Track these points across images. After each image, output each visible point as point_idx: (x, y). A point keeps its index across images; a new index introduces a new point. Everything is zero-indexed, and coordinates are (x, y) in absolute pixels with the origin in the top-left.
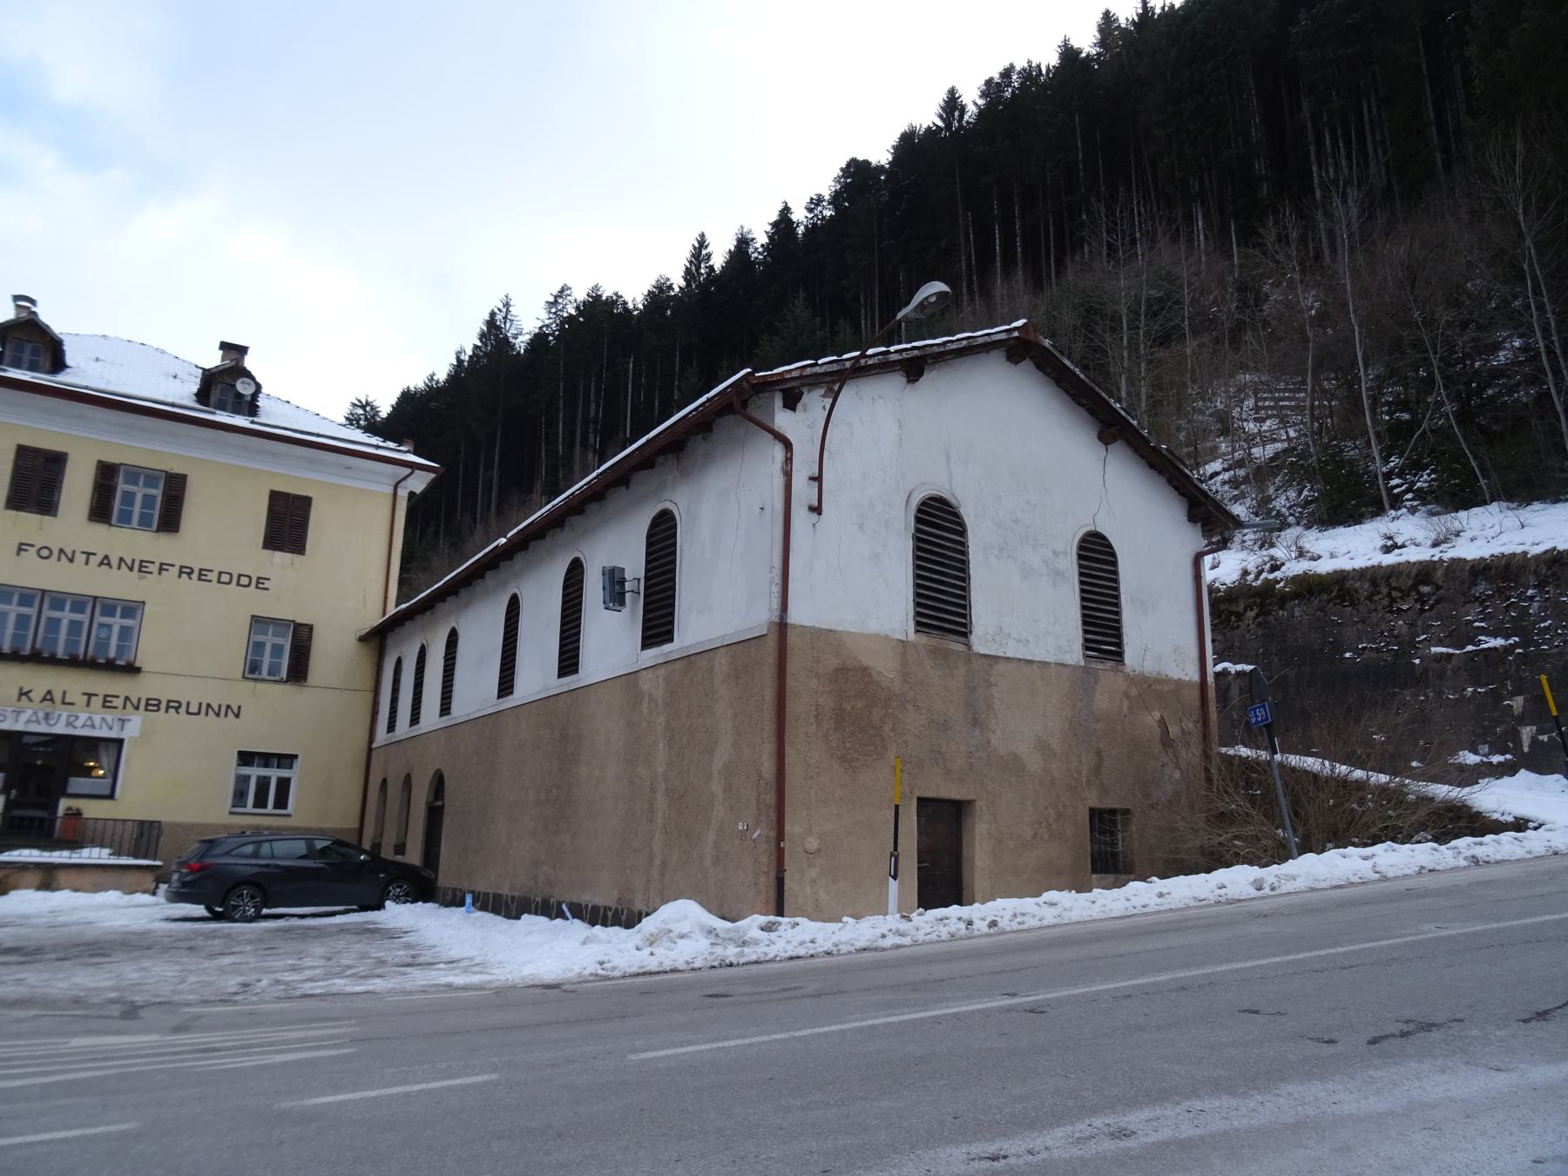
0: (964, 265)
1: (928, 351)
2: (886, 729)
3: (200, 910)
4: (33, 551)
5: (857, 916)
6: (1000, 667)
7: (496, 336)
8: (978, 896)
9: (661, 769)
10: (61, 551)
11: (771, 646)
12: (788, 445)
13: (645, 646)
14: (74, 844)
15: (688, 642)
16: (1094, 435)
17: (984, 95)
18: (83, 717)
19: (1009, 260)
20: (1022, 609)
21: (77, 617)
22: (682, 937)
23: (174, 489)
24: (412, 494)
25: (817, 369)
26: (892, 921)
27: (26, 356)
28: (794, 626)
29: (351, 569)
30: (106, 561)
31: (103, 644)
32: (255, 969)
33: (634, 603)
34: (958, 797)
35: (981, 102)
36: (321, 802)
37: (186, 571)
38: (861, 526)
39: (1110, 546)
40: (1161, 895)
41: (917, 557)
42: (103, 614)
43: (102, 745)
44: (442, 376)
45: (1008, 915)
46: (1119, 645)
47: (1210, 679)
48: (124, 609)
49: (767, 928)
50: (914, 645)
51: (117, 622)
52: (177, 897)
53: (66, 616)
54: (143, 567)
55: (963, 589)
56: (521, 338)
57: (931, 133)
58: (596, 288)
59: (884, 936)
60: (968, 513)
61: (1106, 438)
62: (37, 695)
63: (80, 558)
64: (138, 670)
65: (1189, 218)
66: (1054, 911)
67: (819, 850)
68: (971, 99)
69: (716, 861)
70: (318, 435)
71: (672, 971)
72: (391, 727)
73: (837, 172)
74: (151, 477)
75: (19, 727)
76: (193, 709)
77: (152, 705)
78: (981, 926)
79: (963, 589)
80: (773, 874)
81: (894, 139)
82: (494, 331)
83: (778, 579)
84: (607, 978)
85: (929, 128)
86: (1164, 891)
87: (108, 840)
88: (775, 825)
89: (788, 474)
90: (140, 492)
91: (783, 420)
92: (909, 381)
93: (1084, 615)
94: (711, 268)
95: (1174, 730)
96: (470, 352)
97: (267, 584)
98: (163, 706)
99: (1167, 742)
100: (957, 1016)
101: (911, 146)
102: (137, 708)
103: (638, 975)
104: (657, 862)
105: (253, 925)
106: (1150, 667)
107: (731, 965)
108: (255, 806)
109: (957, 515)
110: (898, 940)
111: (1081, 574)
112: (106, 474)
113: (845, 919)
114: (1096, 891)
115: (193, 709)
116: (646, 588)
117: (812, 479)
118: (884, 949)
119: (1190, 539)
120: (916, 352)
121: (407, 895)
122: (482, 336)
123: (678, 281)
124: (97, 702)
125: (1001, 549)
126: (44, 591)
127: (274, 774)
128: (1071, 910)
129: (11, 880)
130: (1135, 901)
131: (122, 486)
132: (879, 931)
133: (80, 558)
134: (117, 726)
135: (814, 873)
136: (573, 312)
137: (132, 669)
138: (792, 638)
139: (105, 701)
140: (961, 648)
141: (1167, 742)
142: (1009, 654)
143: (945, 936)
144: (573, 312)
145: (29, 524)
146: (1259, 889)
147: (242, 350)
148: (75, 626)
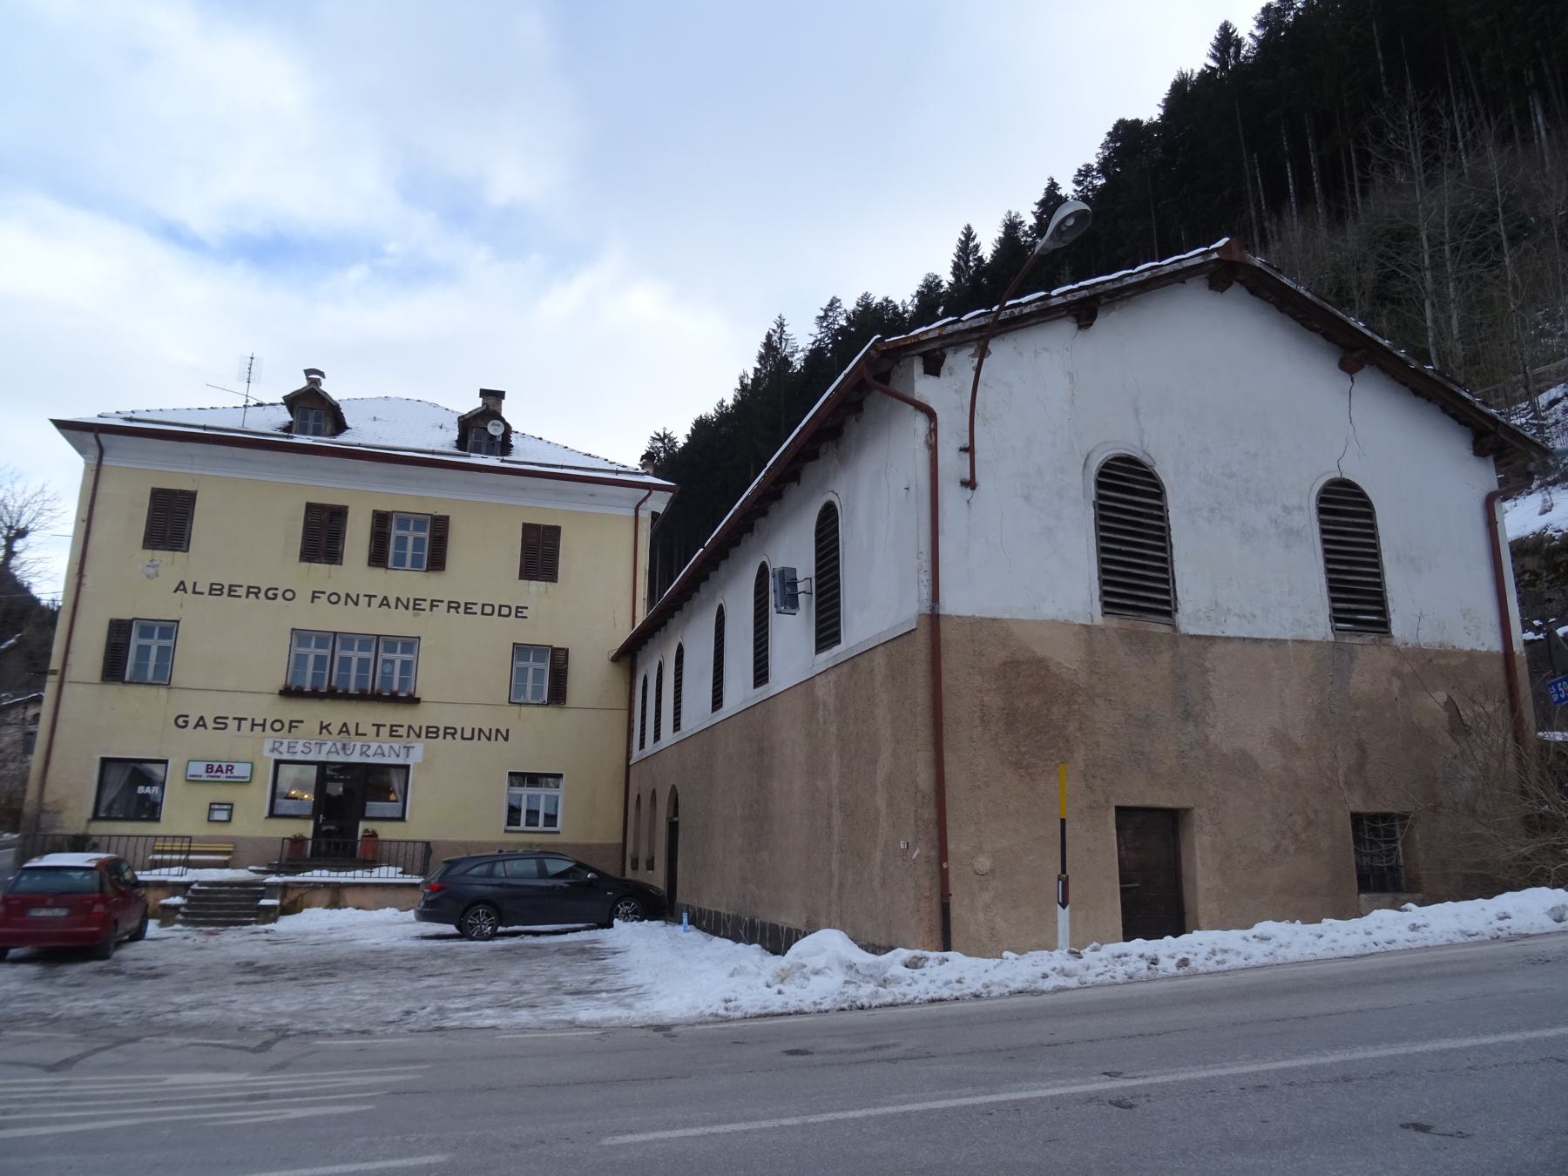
0: (1253, 214)
1: (1100, 289)
2: (1071, 728)
3: (451, 929)
5: (1020, 951)
6: (1217, 649)
7: (774, 357)
8: (1202, 922)
9: (835, 783)
10: (348, 595)
11: (922, 639)
12: (931, 415)
13: (819, 650)
14: (370, 864)
15: (852, 644)
16: (1335, 364)
17: (1261, 24)
18: (374, 746)
19: (1305, 196)
20: (1246, 578)
21: (365, 655)
22: (817, 973)
23: (439, 528)
24: (654, 515)
25: (959, 326)
26: (1060, 958)
27: (311, 423)
28: (949, 617)
29: (601, 591)
30: (385, 602)
31: (387, 678)
32: (408, 996)
33: (809, 604)
34: (1169, 805)
35: (1258, 33)
36: (585, 819)
37: (453, 606)
38: (1027, 498)
39: (1363, 494)
40: (1414, 928)
41: (1100, 528)
42: (343, 648)
43: (393, 771)
44: (729, 402)
45: (1206, 949)
46: (1383, 612)
47: (1518, 648)
48: (404, 644)
49: (913, 964)
50: (1103, 630)
51: (398, 657)
52: (424, 916)
53: (355, 655)
54: (416, 605)
55: (1164, 560)
56: (797, 356)
57: (1206, 76)
58: (866, 296)
59: (1045, 976)
60: (1166, 472)
61: (1349, 366)
62: (335, 729)
64: (418, 701)
65: (1525, 116)
66: (1266, 947)
67: (992, 871)
68: (1247, 29)
69: (883, 885)
70: (562, 467)
71: (797, 1013)
72: (642, 746)
73: (1103, 138)
74: (419, 521)
76: (468, 734)
77: (432, 732)
78: (1168, 966)
79: (1164, 560)
80: (936, 899)
81: (1163, 90)
82: (772, 351)
83: (927, 566)
84: (727, 1020)
85: (1203, 73)
86: (1419, 922)
87: (401, 860)
88: (936, 843)
89: (933, 448)
90: (411, 535)
91: (925, 388)
92: (1080, 327)
93: (1330, 580)
94: (980, 259)
95: (1467, 714)
96: (751, 376)
98: (441, 733)
99: (1458, 726)
100: (1017, 1106)
101: (1183, 95)
102: (419, 736)
103: (760, 1016)
104: (836, 884)
105: (490, 943)
106: (1428, 637)
107: (862, 1008)
108: (528, 824)
109: (1151, 475)
110: (1061, 981)
111: (1323, 531)
112: (381, 521)
113: (1005, 954)
114: (1326, 921)
115: (468, 734)
116: (818, 587)
117: (963, 450)
118: (1043, 992)
119: (1484, 477)
120: (1084, 293)
121: (635, 912)
122: (761, 358)
123: (947, 278)
124: (385, 731)
125: (1213, 510)
126: (335, 634)
128: (1288, 945)
129: (306, 898)
130: (1380, 936)
131: (395, 532)
132: (1040, 970)
133: (363, 601)
134: (403, 752)
135: (987, 897)
136: (844, 323)
137: (413, 700)
138: (947, 631)
140: (1164, 629)
141: (1458, 726)
142: (1229, 633)
143: (1120, 978)
144: (844, 323)
145: (320, 573)
146: (1559, 920)
147: (499, 395)
148: (363, 663)
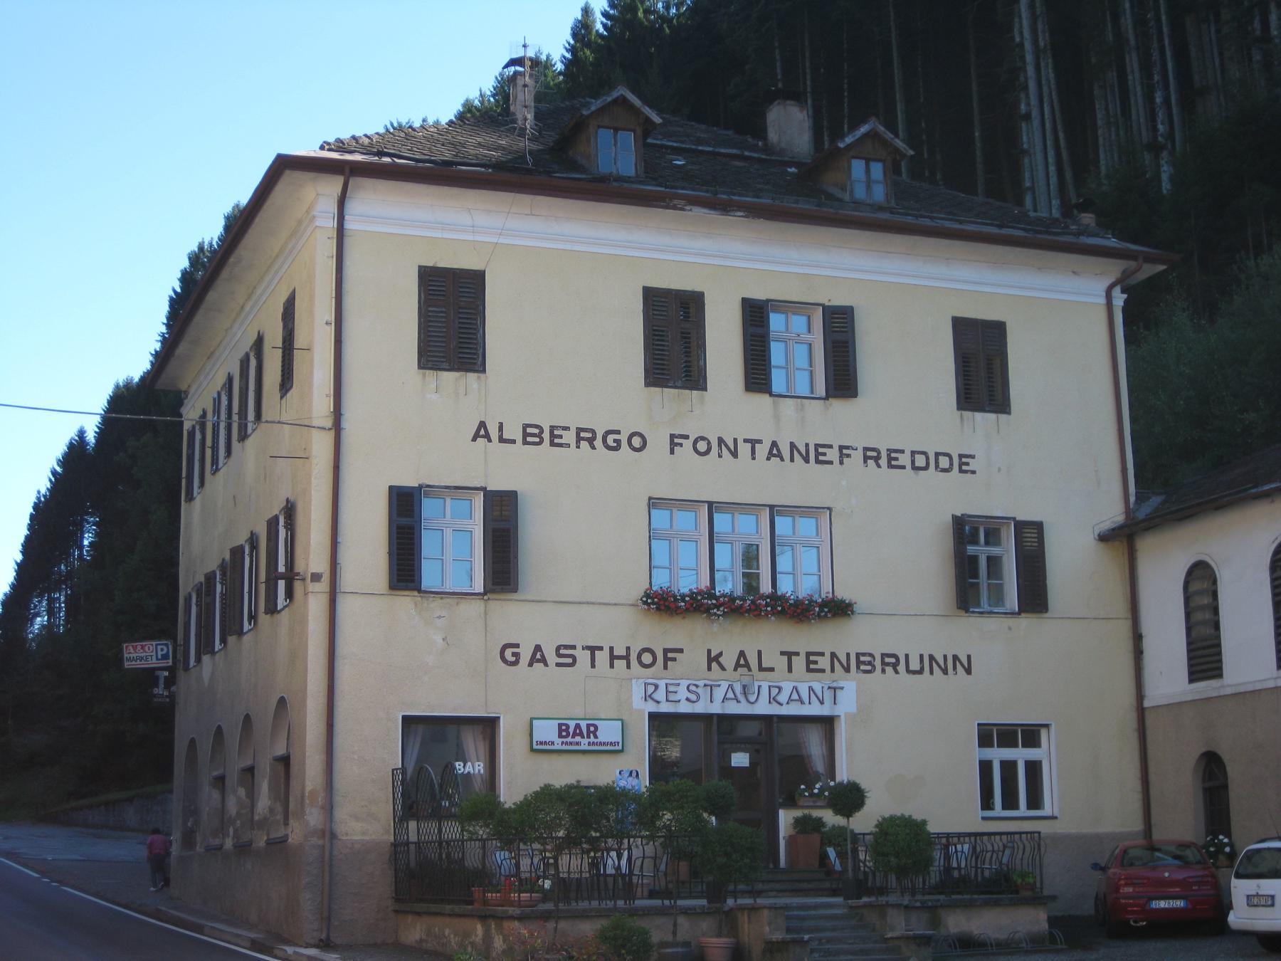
4: (688, 444)
18: (787, 687)
62: (729, 660)
63: (744, 449)
75: (716, 708)
76: (915, 665)
77: (864, 663)
97: (973, 465)
108: (1004, 808)
112: (755, 315)
115: (915, 665)
127: (1020, 755)
131: (776, 322)
133: (744, 449)
134: (828, 696)
139: (809, 662)
